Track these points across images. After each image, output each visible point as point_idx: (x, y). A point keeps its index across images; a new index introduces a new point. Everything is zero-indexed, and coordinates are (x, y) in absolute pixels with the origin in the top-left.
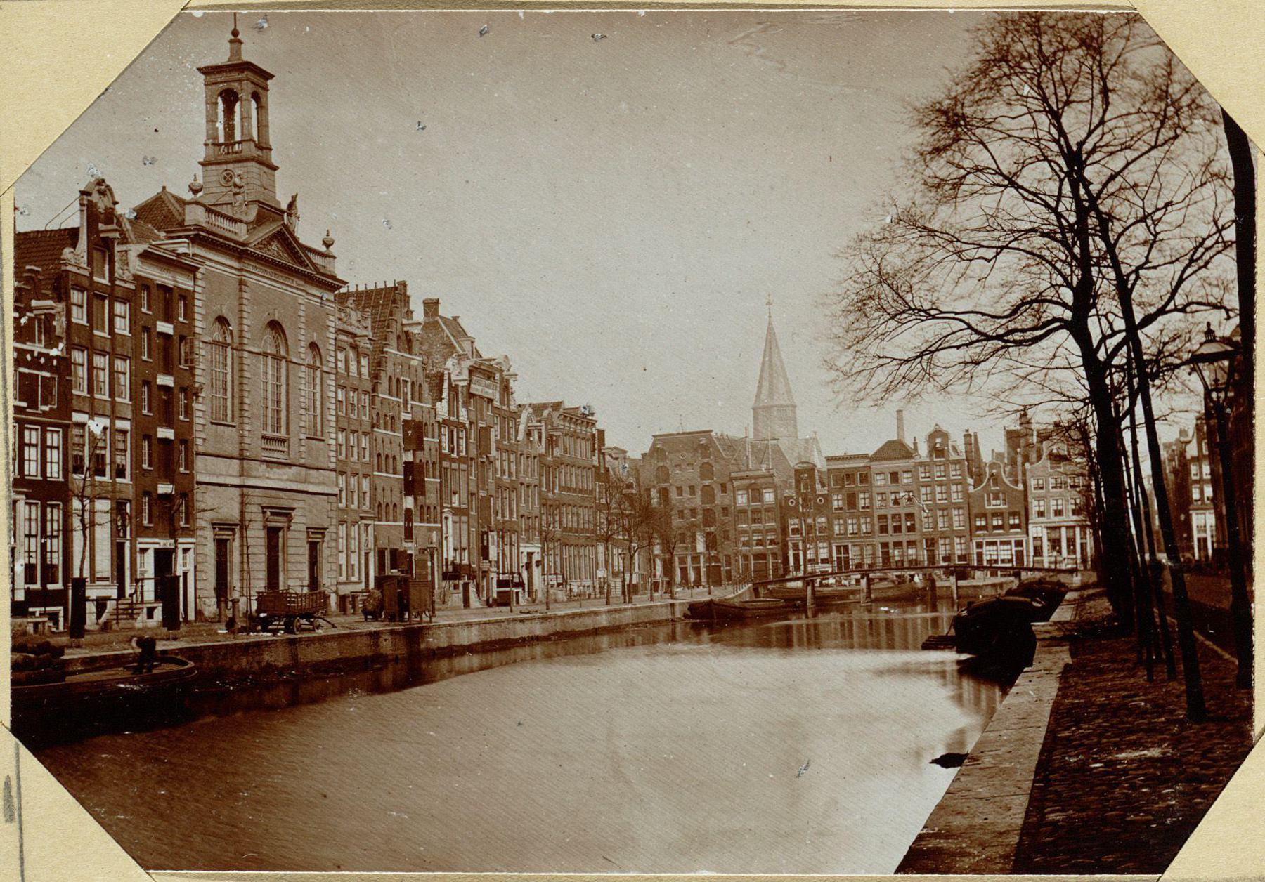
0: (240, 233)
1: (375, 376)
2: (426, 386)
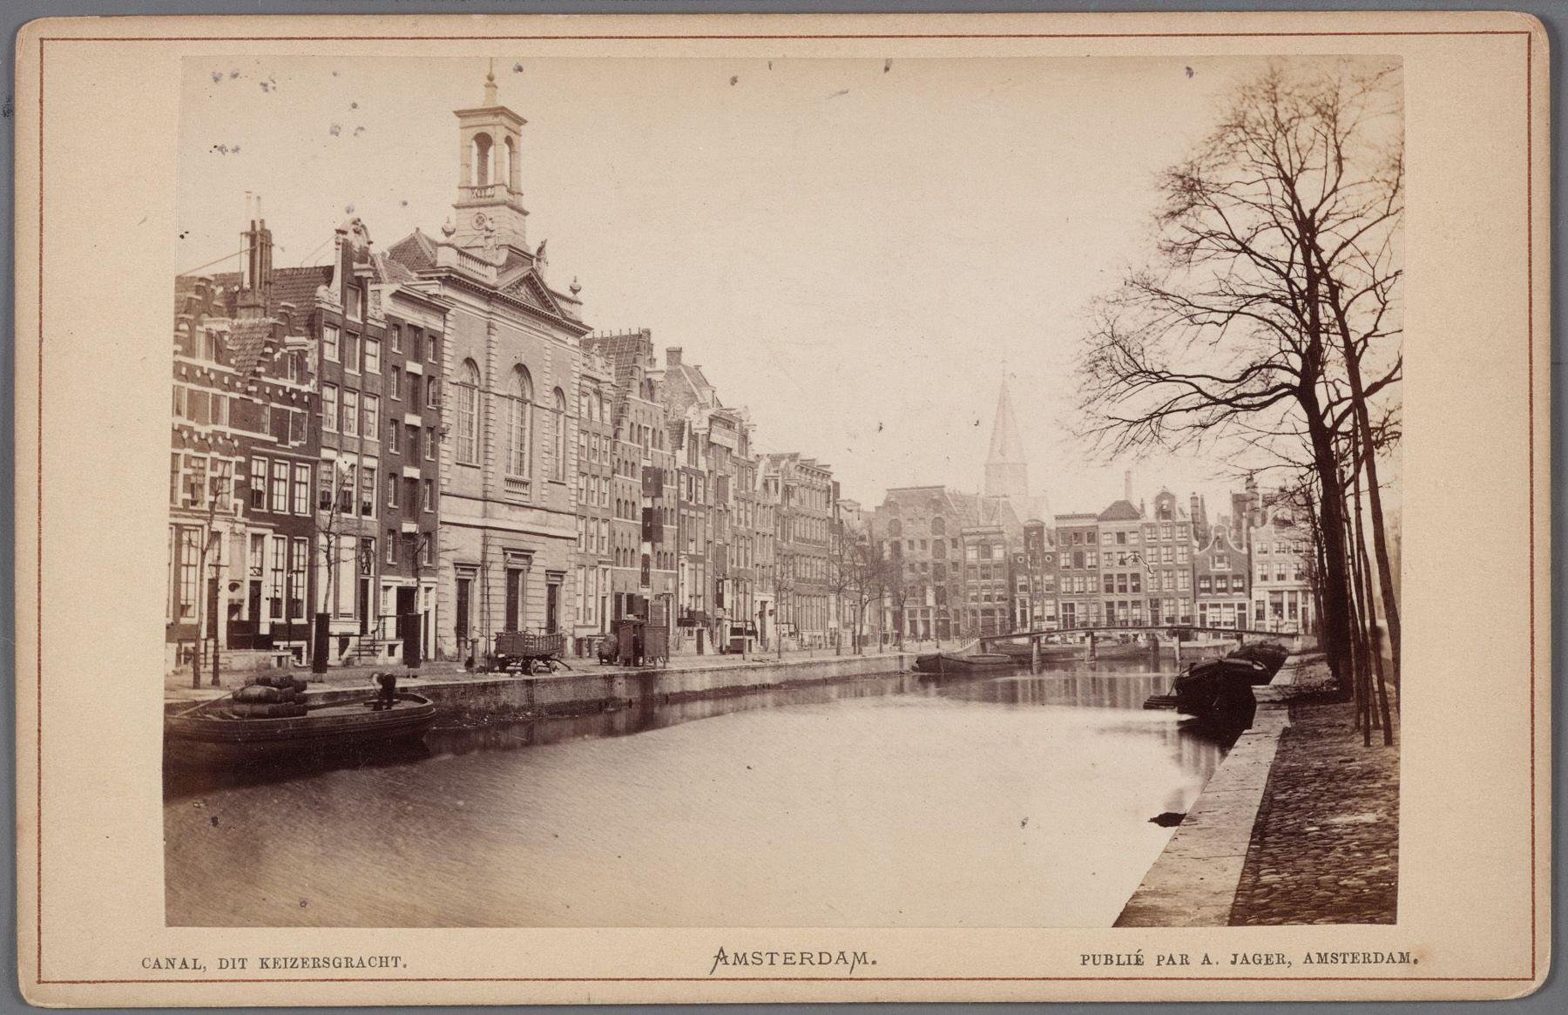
0: (490, 277)
1: (617, 422)
2: (666, 434)
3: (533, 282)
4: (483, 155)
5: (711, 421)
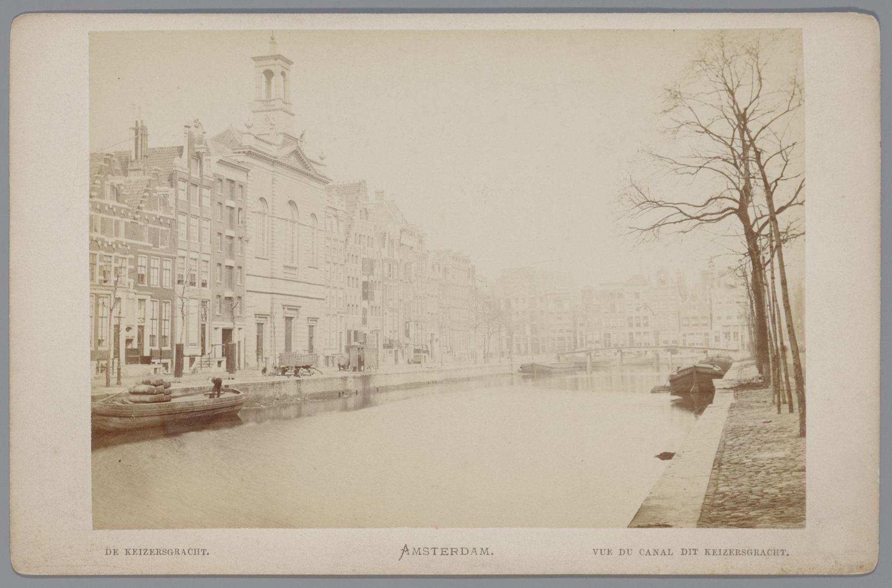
0: (273, 151)
3: (297, 153)
4: (269, 82)
5: (401, 231)
